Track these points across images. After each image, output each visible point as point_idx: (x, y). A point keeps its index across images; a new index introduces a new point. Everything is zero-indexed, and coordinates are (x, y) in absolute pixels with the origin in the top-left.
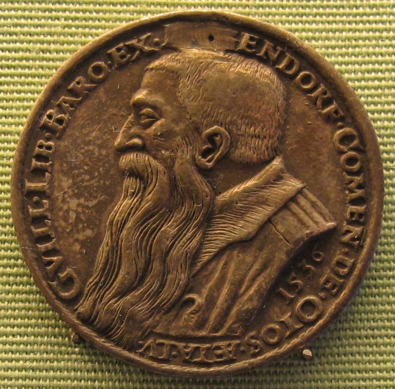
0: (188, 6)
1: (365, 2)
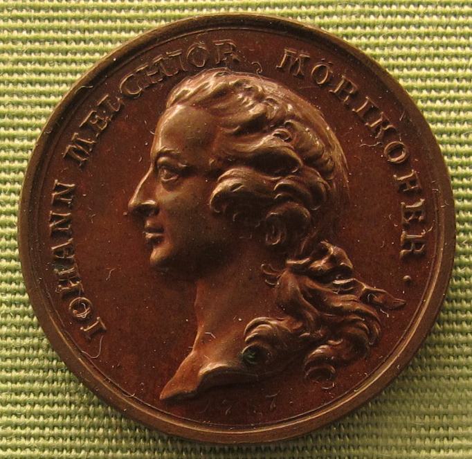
0: (201, 8)
1: (91, 2)
